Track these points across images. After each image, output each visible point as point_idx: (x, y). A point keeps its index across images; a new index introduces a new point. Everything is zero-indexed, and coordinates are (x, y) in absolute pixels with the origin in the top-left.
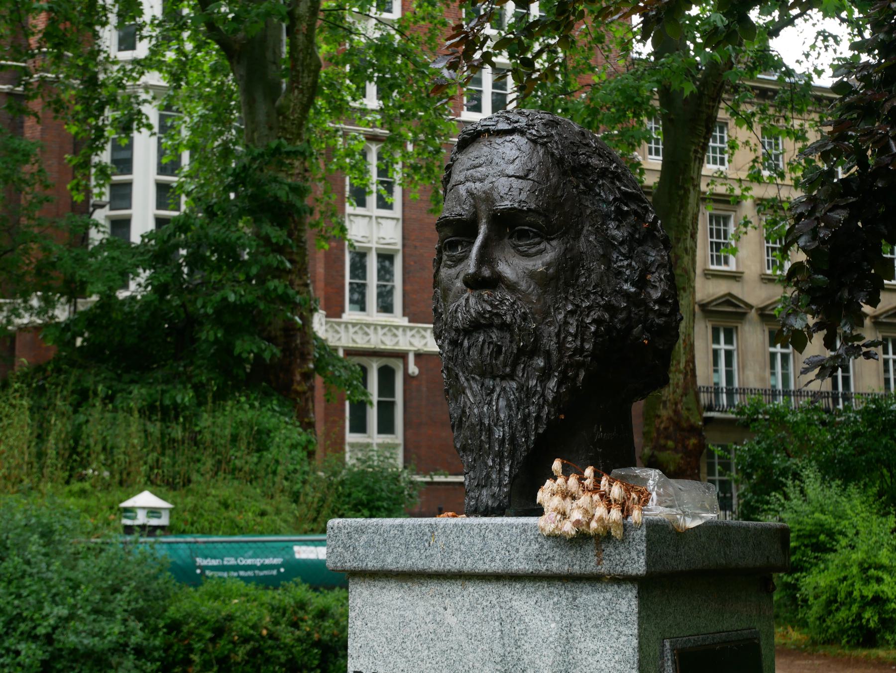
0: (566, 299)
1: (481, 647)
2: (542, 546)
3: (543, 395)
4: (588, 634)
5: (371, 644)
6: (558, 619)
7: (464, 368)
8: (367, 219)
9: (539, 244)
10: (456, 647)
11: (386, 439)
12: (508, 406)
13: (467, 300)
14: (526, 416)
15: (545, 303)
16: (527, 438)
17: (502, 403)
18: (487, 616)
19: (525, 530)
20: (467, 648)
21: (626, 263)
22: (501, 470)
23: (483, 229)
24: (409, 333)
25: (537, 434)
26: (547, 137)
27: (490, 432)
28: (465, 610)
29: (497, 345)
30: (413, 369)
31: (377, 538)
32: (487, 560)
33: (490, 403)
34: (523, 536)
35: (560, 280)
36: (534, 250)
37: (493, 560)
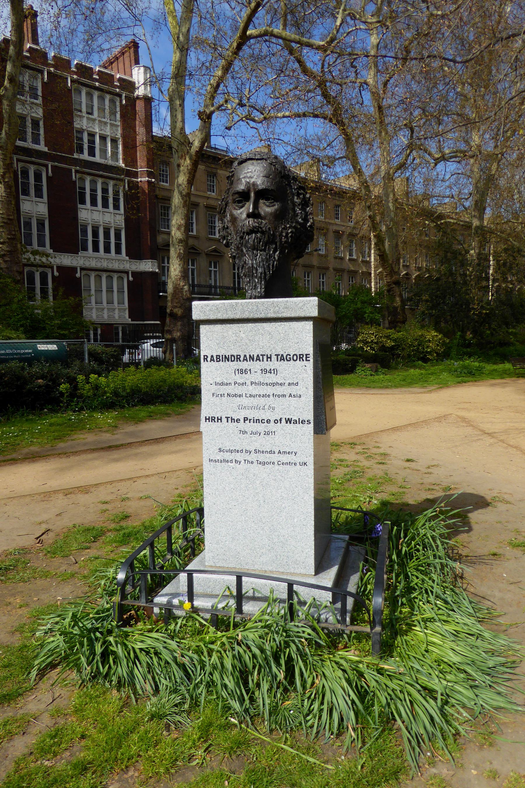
3: (274, 258)
7: (246, 246)
8: (30, 202)
20: (249, 344)
27: (257, 270)
30: (56, 274)
31: (214, 308)
33: (256, 260)
35: (279, 216)
37: (261, 313)
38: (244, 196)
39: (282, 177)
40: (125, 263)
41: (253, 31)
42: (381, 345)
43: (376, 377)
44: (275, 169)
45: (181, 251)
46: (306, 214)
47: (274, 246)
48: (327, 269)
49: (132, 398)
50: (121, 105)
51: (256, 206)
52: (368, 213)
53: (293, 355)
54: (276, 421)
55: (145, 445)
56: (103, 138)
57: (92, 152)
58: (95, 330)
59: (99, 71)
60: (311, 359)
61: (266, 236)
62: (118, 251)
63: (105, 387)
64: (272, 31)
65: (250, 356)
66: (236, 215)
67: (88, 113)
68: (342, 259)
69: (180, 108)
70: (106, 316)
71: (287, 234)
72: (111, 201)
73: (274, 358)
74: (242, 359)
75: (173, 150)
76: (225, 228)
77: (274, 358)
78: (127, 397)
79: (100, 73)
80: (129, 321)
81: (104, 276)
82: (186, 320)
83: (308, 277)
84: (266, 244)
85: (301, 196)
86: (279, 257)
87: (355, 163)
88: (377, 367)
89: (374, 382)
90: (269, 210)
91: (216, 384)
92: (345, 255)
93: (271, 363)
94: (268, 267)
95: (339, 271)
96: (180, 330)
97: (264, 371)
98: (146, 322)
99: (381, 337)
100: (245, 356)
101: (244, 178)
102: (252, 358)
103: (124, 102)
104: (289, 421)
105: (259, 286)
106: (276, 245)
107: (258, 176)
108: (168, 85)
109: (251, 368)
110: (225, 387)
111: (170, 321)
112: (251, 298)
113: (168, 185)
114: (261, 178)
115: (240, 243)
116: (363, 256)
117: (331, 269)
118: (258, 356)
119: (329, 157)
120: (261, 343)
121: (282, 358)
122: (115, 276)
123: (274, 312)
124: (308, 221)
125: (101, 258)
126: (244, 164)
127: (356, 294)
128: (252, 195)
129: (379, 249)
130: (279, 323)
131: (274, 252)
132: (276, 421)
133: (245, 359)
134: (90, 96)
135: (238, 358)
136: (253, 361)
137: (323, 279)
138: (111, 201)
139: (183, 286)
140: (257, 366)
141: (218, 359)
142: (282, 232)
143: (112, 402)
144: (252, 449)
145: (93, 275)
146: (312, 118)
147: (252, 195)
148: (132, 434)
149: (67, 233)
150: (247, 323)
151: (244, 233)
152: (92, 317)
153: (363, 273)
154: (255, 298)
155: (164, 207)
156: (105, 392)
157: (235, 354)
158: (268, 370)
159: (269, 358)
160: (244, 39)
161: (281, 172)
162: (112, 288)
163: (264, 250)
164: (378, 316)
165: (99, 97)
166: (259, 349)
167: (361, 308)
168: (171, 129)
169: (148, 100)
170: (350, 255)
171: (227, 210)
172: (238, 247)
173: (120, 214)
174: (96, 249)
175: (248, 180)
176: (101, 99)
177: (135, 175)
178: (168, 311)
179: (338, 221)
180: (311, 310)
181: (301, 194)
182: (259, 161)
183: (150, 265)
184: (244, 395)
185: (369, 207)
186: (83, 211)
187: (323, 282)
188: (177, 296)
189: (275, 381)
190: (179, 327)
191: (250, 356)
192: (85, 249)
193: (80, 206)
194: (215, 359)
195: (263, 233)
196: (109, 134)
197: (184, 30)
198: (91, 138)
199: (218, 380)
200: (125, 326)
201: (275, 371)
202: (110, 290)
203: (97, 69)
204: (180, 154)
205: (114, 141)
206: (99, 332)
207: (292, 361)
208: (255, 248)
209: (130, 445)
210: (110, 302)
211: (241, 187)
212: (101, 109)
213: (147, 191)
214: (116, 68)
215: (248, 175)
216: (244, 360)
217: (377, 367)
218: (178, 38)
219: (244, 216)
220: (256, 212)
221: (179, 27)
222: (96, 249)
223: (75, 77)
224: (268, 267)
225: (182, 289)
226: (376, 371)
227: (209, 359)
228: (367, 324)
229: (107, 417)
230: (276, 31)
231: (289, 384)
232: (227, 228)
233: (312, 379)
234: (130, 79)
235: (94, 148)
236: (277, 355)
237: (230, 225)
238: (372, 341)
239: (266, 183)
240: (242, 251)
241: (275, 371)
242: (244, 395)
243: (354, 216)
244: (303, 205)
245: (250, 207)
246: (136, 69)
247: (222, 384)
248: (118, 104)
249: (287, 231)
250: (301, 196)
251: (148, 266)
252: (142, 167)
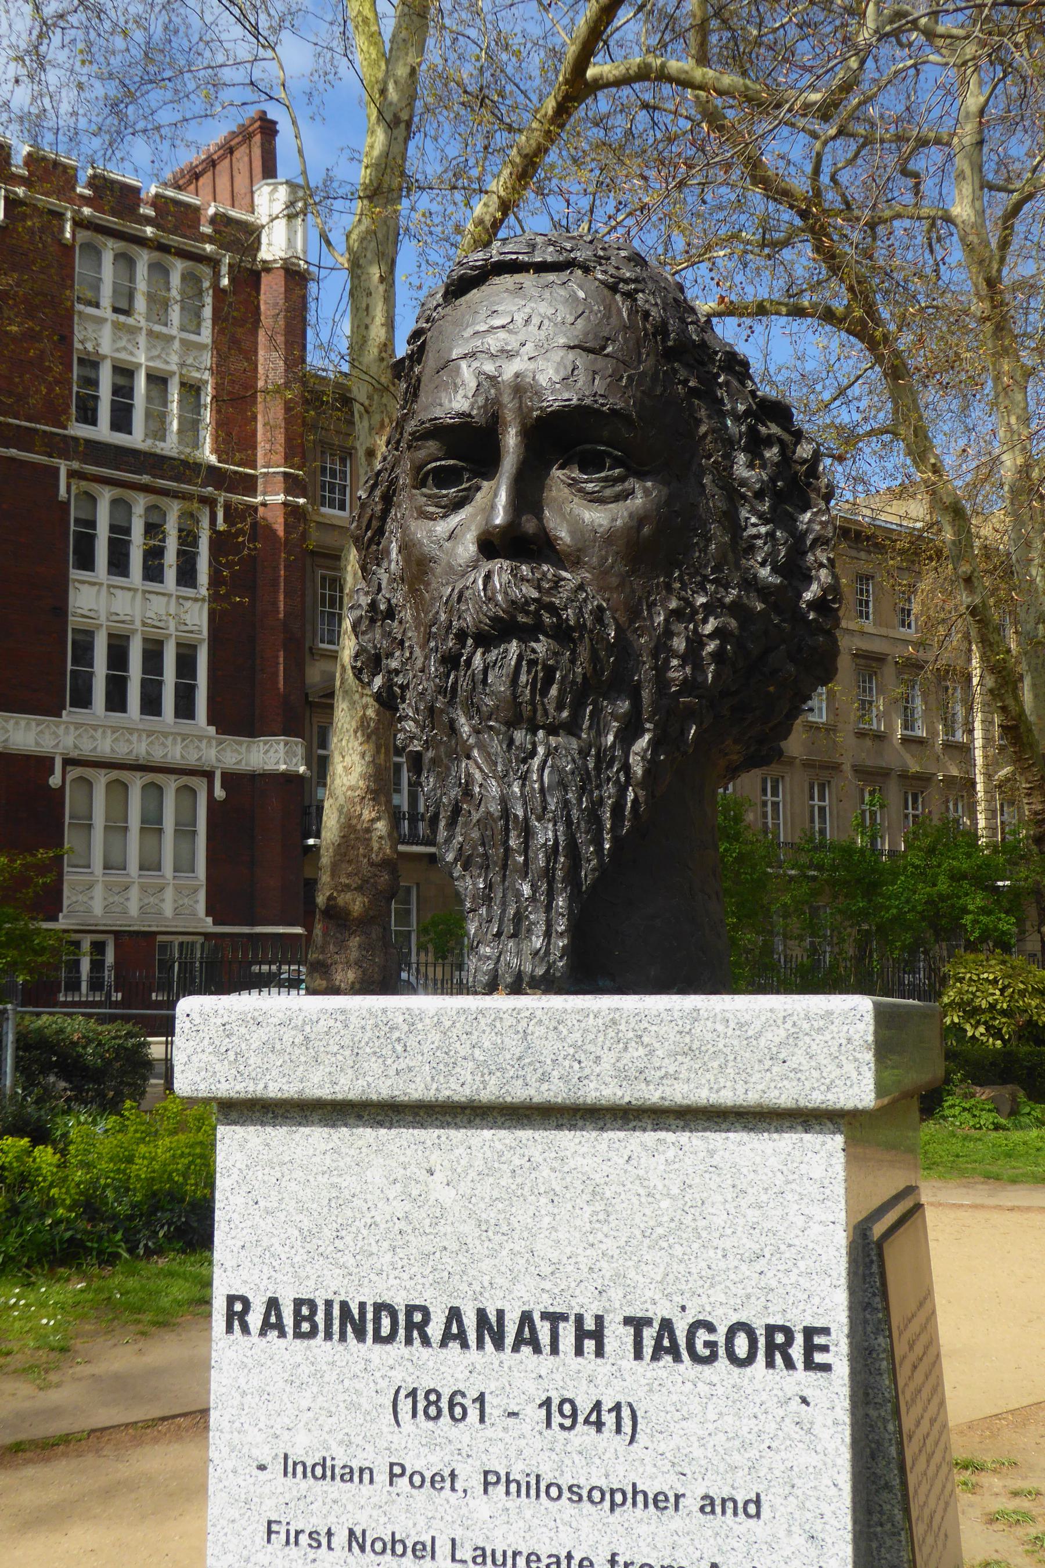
0: (668, 587)
1: (509, 1246)
2: (651, 1052)
3: (626, 767)
4: (741, 1221)
5: (265, 1243)
6: (675, 1191)
7: (472, 708)
9: (622, 479)
10: (455, 1246)
13: (488, 577)
15: (633, 591)
16: (598, 843)
18: (521, 1186)
19: (614, 1022)
21: (763, 530)
25: (615, 840)
26: (635, 281)
27: (527, 833)
28: (472, 1174)
29: (545, 667)
31: (288, 1035)
32: (532, 1079)
33: (524, 778)
34: (611, 1033)
35: (652, 553)
36: (608, 492)
37: (544, 1078)
38: (469, 448)
39: (669, 355)
40: (204, 745)
41: (606, 68)
42: (1022, 1020)
43: (1017, 1136)
44: (633, 312)
45: (370, 713)
46: (798, 546)
47: (624, 706)
48: (836, 767)
49: (148, 1224)
50: (219, 293)
51: (527, 495)
52: (964, 598)
53: (732, 1332)
55: (156, 1440)
56: (158, 381)
57: (122, 420)
58: (98, 948)
59: (157, 196)
60: (838, 1354)
61: (584, 653)
62: (185, 708)
63: (51, 1186)
64: (663, 65)
65: (481, 1314)
66: (430, 548)
67: (116, 310)
68: (879, 737)
69: (382, 288)
70: (134, 909)
71: (696, 642)
72: (170, 557)
73: (618, 1337)
74: (435, 1330)
75: (357, 407)
76: (379, 615)
77: (618, 1337)
78: (130, 1218)
79: (158, 202)
80: (208, 924)
81: (136, 783)
82: (375, 932)
83: (775, 793)
84: (584, 693)
85: (772, 453)
86: (652, 768)
87: (920, 450)
88: (1014, 1100)
89: (1009, 1155)
90: (597, 517)
91: (290, 1467)
92: (890, 725)
93: (602, 1368)
94: (593, 816)
95: (873, 776)
96: (358, 963)
97: (560, 1412)
99: (1022, 993)
100: (455, 1314)
101: (472, 355)
102: (490, 1328)
103: (225, 282)
105: (537, 917)
106: (635, 697)
107: (543, 350)
108: (348, 220)
109: (489, 1387)
110: (335, 1489)
111: (325, 934)
112: (491, 988)
114: (557, 355)
115: (441, 690)
116: (950, 729)
117: (847, 768)
118: (526, 1318)
119: (840, 429)
120: (542, 1246)
121: (667, 1346)
122: (171, 785)
123: (622, 1075)
124: (808, 580)
125: (131, 731)
126: (474, 294)
127: (931, 851)
128: (511, 439)
129: (1004, 709)
130: (650, 1137)
131: (629, 733)
133: (454, 1333)
134: (126, 261)
135: (413, 1324)
136: (499, 1345)
137: (822, 798)
138: (170, 557)
139: (373, 821)
141: (307, 1320)
142: (668, 634)
143: (72, 1239)
145: (101, 780)
146: (784, 320)
147: (511, 439)
148: (121, 1386)
150: (469, 1124)
151: (462, 636)
152: (89, 911)
153: (949, 780)
154: (516, 989)
156: (52, 1203)
157: (400, 1302)
158: (584, 1406)
159: (591, 1336)
160: (578, 88)
161: (662, 329)
162: (160, 821)
163: (571, 728)
164: (1007, 924)
165: (153, 267)
166: (531, 1282)
167: (949, 897)
168: (351, 347)
169: (296, 277)
170: (906, 727)
171: (390, 526)
172: (431, 710)
173: (196, 600)
174: (116, 701)
175: (489, 368)
176: (160, 271)
177: (249, 484)
178: (321, 900)
179: (868, 626)
180: (831, 1071)
181: (769, 441)
182: (551, 277)
183: (281, 754)
184: (443, 1549)
185: (968, 580)
186: (85, 588)
187: (822, 809)
188: (352, 854)
189: (620, 1478)
190: (354, 955)
191: (481, 1314)
192: (83, 699)
193: (75, 574)
194: (288, 1321)
195: (563, 634)
196: (174, 368)
197: (402, 71)
198: (121, 381)
199: (304, 1447)
201: (620, 1418)
202: (152, 824)
203: (153, 190)
204: (376, 418)
205: (191, 389)
206: (110, 958)
207: (723, 1362)
208: (518, 715)
209: (97, 1437)
210: (150, 864)
211: (458, 401)
212: (159, 304)
213: (281, 533)
214: (210, 188)
215: (493, 343)
216: (446, 1338)
217: (1014, 1100)
218: (383, 92)
219: (467, 548)
220: (529, 525)
221: (388, 62)
222: (116, 701)
223: (87, 211)
224: (593, 816)
225: (368, 830)
226: (1014, 1113)
227: (255, 1320)
228: (971, 947)
229: (43, 1305)
230: (674, 65)
231: (709, 1505)
232: (390, 613)
233: (848, 1521)
234: (250, 218)
235: (129, 408)
236: (637, 1324)
237: (398, 599)
238: (992, 1007)
239: (582, 379)
240: (453, 729)
241: (620, 1418)
242: (443, 1549)
243: (916, 608)
244: (779, 498)
245: (495, 501)
246: (266, 189)
247: (323, 1470)
249: (692, 628)
250: (772, 453)
251: (274, 755)
252: (269, 463)
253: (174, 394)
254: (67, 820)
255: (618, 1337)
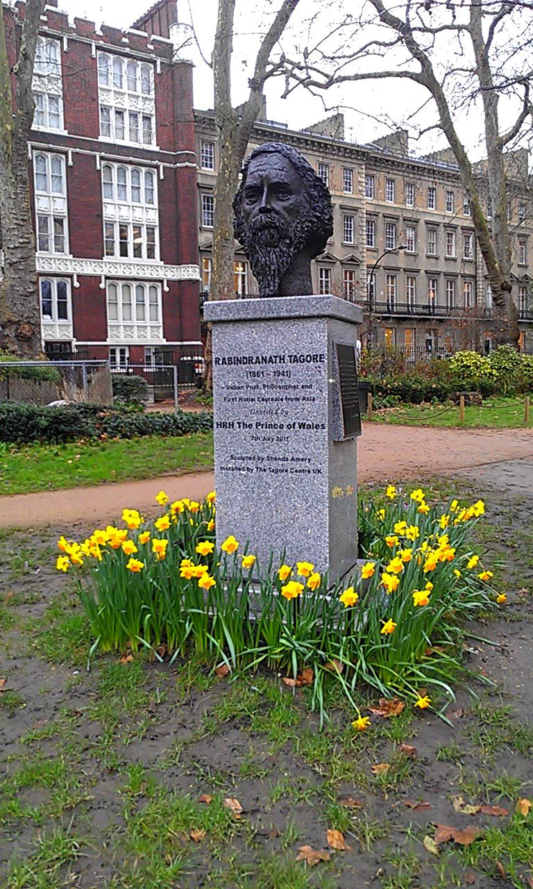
7: (259, 243)
11: (63, 321)
12: (276, 257)
14: (283, 261)
17: (274, 256)
20: (261, 345)
22: (274, 281)
23: (265, 189)
24: (73, 263)
27: (270, 267)
30: (77, 284)
54: (289, 427)
62: (151, 255)
80: (164, 342)
97: (277, 373)
98: (185, 343)
102: (264, 359)
104: (302, 426)
113: (212, 170)
117: (422, 272)
118: (271, 357)
132: (289, 427)
133: (258, 361)
135: (250, 360)
140: (271, 367)
141: (230, 361)
144: (265, 455)
149: (87, 233)
151: (256, 229)
155: (208, 198)
159: (282, 359)
174: (124, 253)
200: (159, 349)
201: (288, 374)
202: (141, 304)
206: (127, 355)
227: (221, 362)
247: (234, 388)
248: (152, 71)
253: (140, 120)
254: (108, 301)
255: (287, 358)
